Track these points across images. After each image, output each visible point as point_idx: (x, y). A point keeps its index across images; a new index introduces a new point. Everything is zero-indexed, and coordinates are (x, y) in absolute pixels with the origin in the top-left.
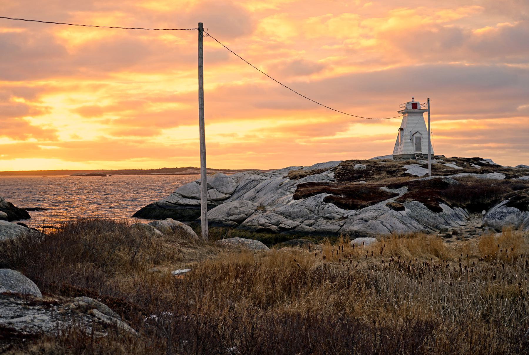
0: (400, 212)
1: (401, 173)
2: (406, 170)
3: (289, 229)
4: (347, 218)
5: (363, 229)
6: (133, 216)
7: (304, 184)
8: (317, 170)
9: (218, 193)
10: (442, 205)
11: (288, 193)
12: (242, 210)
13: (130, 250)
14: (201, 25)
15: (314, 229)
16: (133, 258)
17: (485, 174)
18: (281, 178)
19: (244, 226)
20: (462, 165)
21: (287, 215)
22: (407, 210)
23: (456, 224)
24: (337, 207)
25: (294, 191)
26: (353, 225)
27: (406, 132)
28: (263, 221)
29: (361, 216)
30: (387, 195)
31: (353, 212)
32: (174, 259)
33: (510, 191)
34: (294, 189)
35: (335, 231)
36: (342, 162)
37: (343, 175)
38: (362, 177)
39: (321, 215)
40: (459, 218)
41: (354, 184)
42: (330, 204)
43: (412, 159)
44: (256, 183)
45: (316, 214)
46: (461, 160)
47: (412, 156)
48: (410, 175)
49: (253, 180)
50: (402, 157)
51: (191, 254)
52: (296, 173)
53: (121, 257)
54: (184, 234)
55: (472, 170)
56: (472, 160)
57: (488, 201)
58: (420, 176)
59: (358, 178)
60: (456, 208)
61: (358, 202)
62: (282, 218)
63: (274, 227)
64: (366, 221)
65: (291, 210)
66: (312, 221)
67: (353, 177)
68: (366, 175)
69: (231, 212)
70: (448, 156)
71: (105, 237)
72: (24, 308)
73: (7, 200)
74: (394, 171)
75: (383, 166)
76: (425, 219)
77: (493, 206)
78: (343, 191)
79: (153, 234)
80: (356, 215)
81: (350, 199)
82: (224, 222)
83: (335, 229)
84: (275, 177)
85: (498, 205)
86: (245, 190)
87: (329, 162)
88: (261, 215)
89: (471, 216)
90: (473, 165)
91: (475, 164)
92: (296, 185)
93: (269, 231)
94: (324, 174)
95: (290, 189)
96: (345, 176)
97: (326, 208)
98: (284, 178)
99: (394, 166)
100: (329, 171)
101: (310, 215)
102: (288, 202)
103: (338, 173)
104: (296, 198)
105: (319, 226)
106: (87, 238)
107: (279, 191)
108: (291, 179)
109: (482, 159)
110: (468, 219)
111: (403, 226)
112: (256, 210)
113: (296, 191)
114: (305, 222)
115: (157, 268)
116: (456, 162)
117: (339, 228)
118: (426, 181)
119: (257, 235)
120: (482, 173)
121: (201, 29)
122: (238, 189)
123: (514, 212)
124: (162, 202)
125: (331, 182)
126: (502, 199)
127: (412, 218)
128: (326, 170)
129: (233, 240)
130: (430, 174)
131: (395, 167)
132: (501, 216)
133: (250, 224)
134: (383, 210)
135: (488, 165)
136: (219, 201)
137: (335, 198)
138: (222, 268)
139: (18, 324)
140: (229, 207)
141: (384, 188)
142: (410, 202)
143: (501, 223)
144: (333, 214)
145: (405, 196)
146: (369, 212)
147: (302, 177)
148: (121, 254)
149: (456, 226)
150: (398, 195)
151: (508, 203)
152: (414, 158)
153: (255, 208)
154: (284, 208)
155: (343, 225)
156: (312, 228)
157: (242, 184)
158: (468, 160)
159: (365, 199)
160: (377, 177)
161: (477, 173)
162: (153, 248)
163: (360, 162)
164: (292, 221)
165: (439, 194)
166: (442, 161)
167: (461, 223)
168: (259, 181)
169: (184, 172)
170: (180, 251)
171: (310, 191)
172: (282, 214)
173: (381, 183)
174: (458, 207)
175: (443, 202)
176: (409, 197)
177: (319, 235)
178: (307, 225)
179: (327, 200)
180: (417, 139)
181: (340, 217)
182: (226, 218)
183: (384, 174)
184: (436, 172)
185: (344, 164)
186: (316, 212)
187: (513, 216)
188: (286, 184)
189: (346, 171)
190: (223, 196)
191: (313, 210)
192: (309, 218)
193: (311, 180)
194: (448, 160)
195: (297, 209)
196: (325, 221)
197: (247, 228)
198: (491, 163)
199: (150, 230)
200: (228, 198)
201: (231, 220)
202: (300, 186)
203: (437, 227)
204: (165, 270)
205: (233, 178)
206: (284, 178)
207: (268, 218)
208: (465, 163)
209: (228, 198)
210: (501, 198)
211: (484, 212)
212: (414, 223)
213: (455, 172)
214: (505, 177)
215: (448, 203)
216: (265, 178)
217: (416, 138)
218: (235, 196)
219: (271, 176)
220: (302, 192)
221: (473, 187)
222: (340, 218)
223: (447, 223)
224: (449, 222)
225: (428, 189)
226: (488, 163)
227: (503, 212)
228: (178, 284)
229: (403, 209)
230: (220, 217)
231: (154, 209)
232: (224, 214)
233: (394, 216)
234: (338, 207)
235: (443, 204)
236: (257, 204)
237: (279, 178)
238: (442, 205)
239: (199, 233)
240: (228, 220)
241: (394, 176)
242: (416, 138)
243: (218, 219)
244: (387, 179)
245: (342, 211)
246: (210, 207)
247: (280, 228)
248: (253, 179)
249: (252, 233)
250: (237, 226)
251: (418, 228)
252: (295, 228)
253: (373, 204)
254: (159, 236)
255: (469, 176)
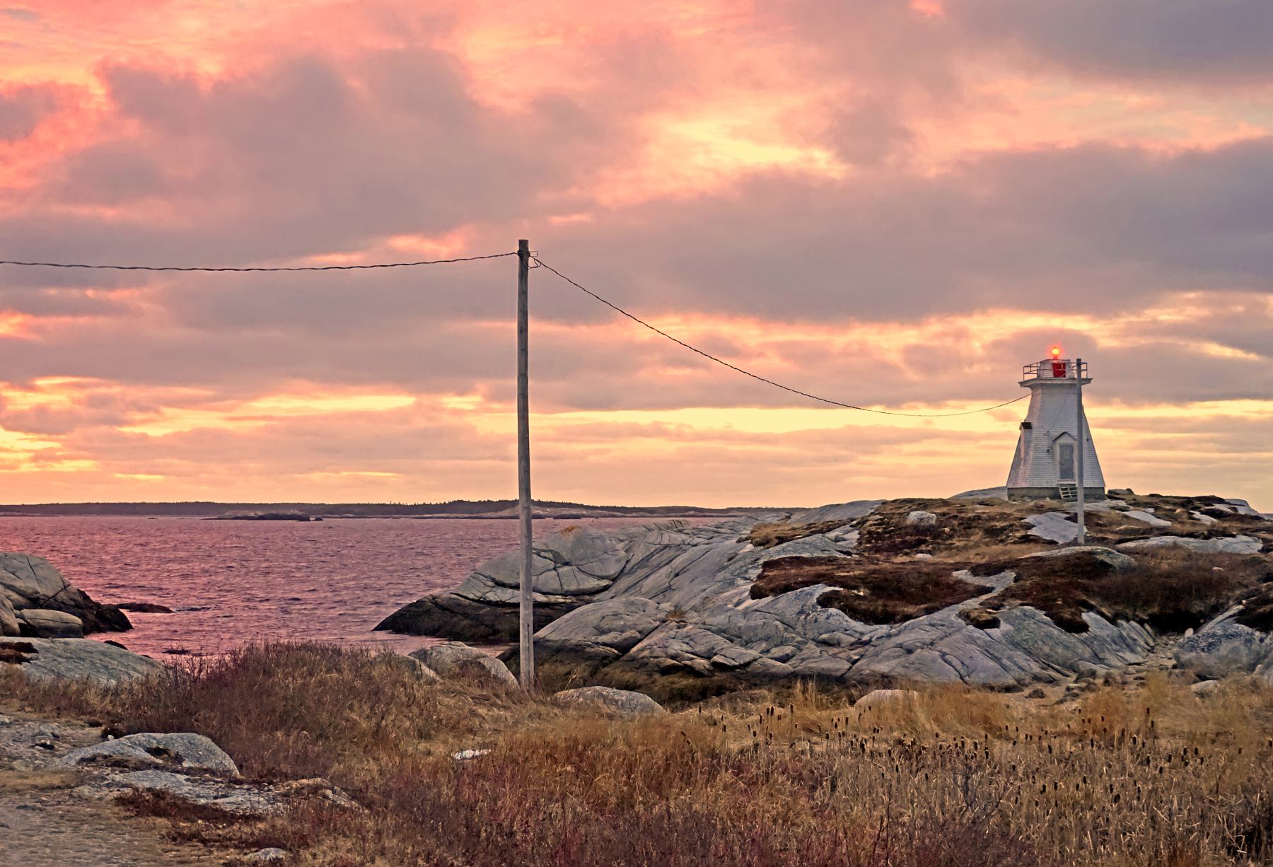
0: (988, 630)
1: (1018, 534)
2: (1030, 527)
3: (735, 667)
4: (868, 643)
5: (900, 670)
6: (382, 627)
7: (785, 556)
8: (821, 522)
9: (584, 576)
10: (1087, 617)
11: (741, 582)
12: (631, 619)
13: (372, 709)
14: (523, 244)
15: (791, 669)
16: (378, 725)
17: (1214, 539)
18: (734, 541)
19: (633, 659)
20: (1169, 516)
21: (732, 636)
22: (1005, 626)
23: (1116, 661)
24: (847, 618)
25: (754, 577)
26: (879, 662)
27: (1035, 432)
28: (676, 647)
29: (899, 640)
30: (966, 592)
31: (884, 629)
32: (459, 729)
33: (1252, 584)
34: (754, 573)
35: (839, 674)
36: (884, 503)
37: (879, 537)
38: (924, 542)
39: (810, 635)
40: (1128, 646)
41: (895, 564)
42: (833, 610)
43: (1051, 498)
44: (671, 553)
45: (798, 634)
46: (1168, 503)
47: (1051, 492)
48: (1036, 540)
49: (666, 546)
50: (1029, 493)
51: (496, 720)
52: (769, 530)
53: (355, 723)
54: (484, 676)
55: (1188, 528)
56: (1197, 504)
57: (1198, 607)
58: (1061, 542)
59: (915, 546)
60: (1124, 623)
61: (896, 606)
62: (719, 640)
63: (701, 663)
64: (910, 651)
65: (742, 623)
66: (788, 649)
67: (903, 542)
68: (935, 538)
69: (605, 625)
70: (1141, 491)
71: (321, 683)
72: (229, 787)
73: (75, 584)
74: (1003, 529)
75: (978, 517)
76: (1046, 649)
77: (1212, 619)
78: (864, 581)
79: (418, 678)
80: (889, 636)
81: (879, 597)
82: (588, 649)
83: (838, 670)
84: (718, 539)
85: (1220, 618)
86: (646, 571)
87: (852, 504)
88: (672, 633)
89: (1159, 641)
90: (1197, 514)
91: (1202, 513)
92: (761, 562)
93: (690, 671)
94: (832, 535)
95: (746, 572)
96: (883, 539)
97: (822, 617)
98: (739, 541)
99: (1003, 516)
100: (847, 527)
101: (787, 635)
102: (738, 604)
103: (869, 532)
104: (756, 594)
105: (803, 660)
106: (287, 683)
107: (720, 576)
108: (757, 544)
109: (1221, 501)
110: (1152, 650)
111: (991, 663)
112: (664, 621)
113: (760, 577)
114: (774, 650)
115: (423, 746)
116: (1156, 508)
117: (847, 665)
118: (1057, 558)
119: (661, 680)
120: (1207, 538)
121: (523, 253)
122: (629, 566)
123: (1240, 635)
124: (445, 595)
125: (842, 556)
126: (1231, 603)
127: (1016, 645)
128: (840, 524)
129: (588, 691)
130: (1081, 540)
131: (1005, 520)
132: (1210, 645)
133: (646, 653)
134: (951, 625)
135: (1236, 517)
136: (584, 596)
137: (845, 596)
138: (546, 745)
139: (225, 804)
140: (599, 614)
141: (958, 575)
142: (1014, 609)
143: (1208, 659)
144: (838, 635)
145: (1008, 594)
146: (919, 630)
147: (781, 540)
148: (354, 716)
149: (1120, 664)
150: (989, 590)
151: (1241, 613)
152: (1056, 496)
153: (662, 615)
154: (723, 615)
155: (857, 661)
156: (787, 667)
157: (639, 554)
158: (1187, 503)
159: (913, 600)
160: (961, 544)
161: (1196, 537)
162: (419, 705)
163: (923, 504)
164: (743, 650)
165: (1086, 589)
166: (1122, 503)
167: (1131, 657)
168: (680, 548)
169: (506, 513)
170: (474, 713)
171: (787, 577)
172: (720, 632)
173: (957, 560)
174: (1128, 620)
175: (1091, 608)
176: (1014, 596)
177: (782, 683)
178: (776, 659)
179: (825, 601)
180: (1074, 447)
181: (853, 640)
182: (593, 638)
183: (977, 536)
184: (1101, 531)
185: (888, 510)
186: (799, 628)
187: (1237, 643)
188: (744, 557)
189: (891, 528)
190: (592, 583)
191: (792, 623)
192: (783, 643)
193: (795, 551)
194: (1138, 503)
195: (757, 620)
196: (818, 650)
197: (640, 664)
198: (1242, 511)
199: (415, 669)
200: (606, 588)
201: (604, 644)
202: (768, 565)
203: (1073, 669)
204: (439, 749)
205: (622, 537)
206: (739, 541)
207: (689, 639)
208: (1178, 511)
209: (606, 588)
210: (1229, 598)
211: (1189, 632)
212: (1020, 657)
213: (1149, 531)
214: (1260, 546)
215: (1104, 610)
216: (696, 540)
217: (1062, 446)
218: (623, 583)
219: (710, 535)
220: (771, 580)
221: (1169, 575)
222: (852, 644)
223: (1097, 658)
224: (1101, 656)
225: (1061, 576)
226: (1235, 509)
227: (1214, 635)
228: (459, 770)
229: (994, 623)
230: (577, 638)
231: (428, 612)
232: (590, 630)
233: (973, 640)
234: (851, 617)
235: (1091, 614)
236: (667, 606)
237: (728, 542)
238: (1087, 617)
239: (517, 674)
240: (597, 644)
241: (1002, 541)
242: (1062, 446)
243: (574, 642)
244: (984, 549)
245: (859, 626)
246: (545, 614)
247: (715, 664)
248: (666, 542)
249: (650, 675)
250: (617, 658)
251: (1027, 668)
252: (747, 664)
253: (929, 611)
254: (432, 682)
255: (1175, 546)
